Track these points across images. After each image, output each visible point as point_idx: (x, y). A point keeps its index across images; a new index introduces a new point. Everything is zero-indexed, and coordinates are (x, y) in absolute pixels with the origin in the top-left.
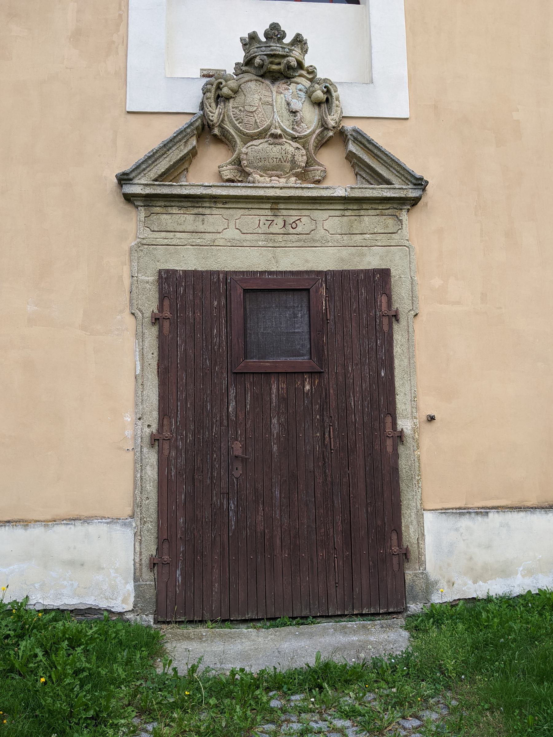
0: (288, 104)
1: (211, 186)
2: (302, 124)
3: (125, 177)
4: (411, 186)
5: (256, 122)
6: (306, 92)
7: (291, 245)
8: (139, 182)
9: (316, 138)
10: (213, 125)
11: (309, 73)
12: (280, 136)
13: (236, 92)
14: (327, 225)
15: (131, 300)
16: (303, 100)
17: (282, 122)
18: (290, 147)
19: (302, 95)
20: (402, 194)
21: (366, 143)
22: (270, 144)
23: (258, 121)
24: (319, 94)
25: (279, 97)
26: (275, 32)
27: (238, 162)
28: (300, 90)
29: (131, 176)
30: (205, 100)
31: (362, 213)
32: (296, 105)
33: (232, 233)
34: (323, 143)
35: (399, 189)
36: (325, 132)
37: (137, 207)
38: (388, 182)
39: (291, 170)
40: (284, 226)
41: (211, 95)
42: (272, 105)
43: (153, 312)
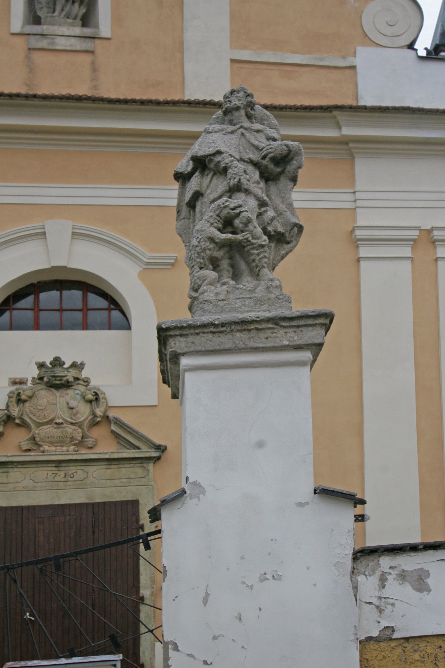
0: (68, 404)
1: (13, 456)
2: (78, 415)
4: (153, 450)
5: (45, 415)
6: (81, 395)
7: (69, 488)
9: (89, 421)
10: (15, 418)
11: (84, 381)
12: (62, 423)
13: (31, 397)
14: (95, 475)
16: (79, 400)
17: (62, 414)
18: (70, 429)
19: (78, 397)
20: (148, 455)
21: (122, 425)
22: (55, 428)
23: (46, 415)
24: (90, 397)
25: (62, 399)
26: (57, 362)
27: (34, 438)
28: (77, 394)
30: (9, 403)
31: (121, 466)
32: (73, 403)
33: (27, 483)
34: (94, 424)
35: (147, 452)
36: (95, 418)
38: (139, 448)
39: (71, 442)
40: (65, 477)
41: (14, 400)
42: (58, 404)
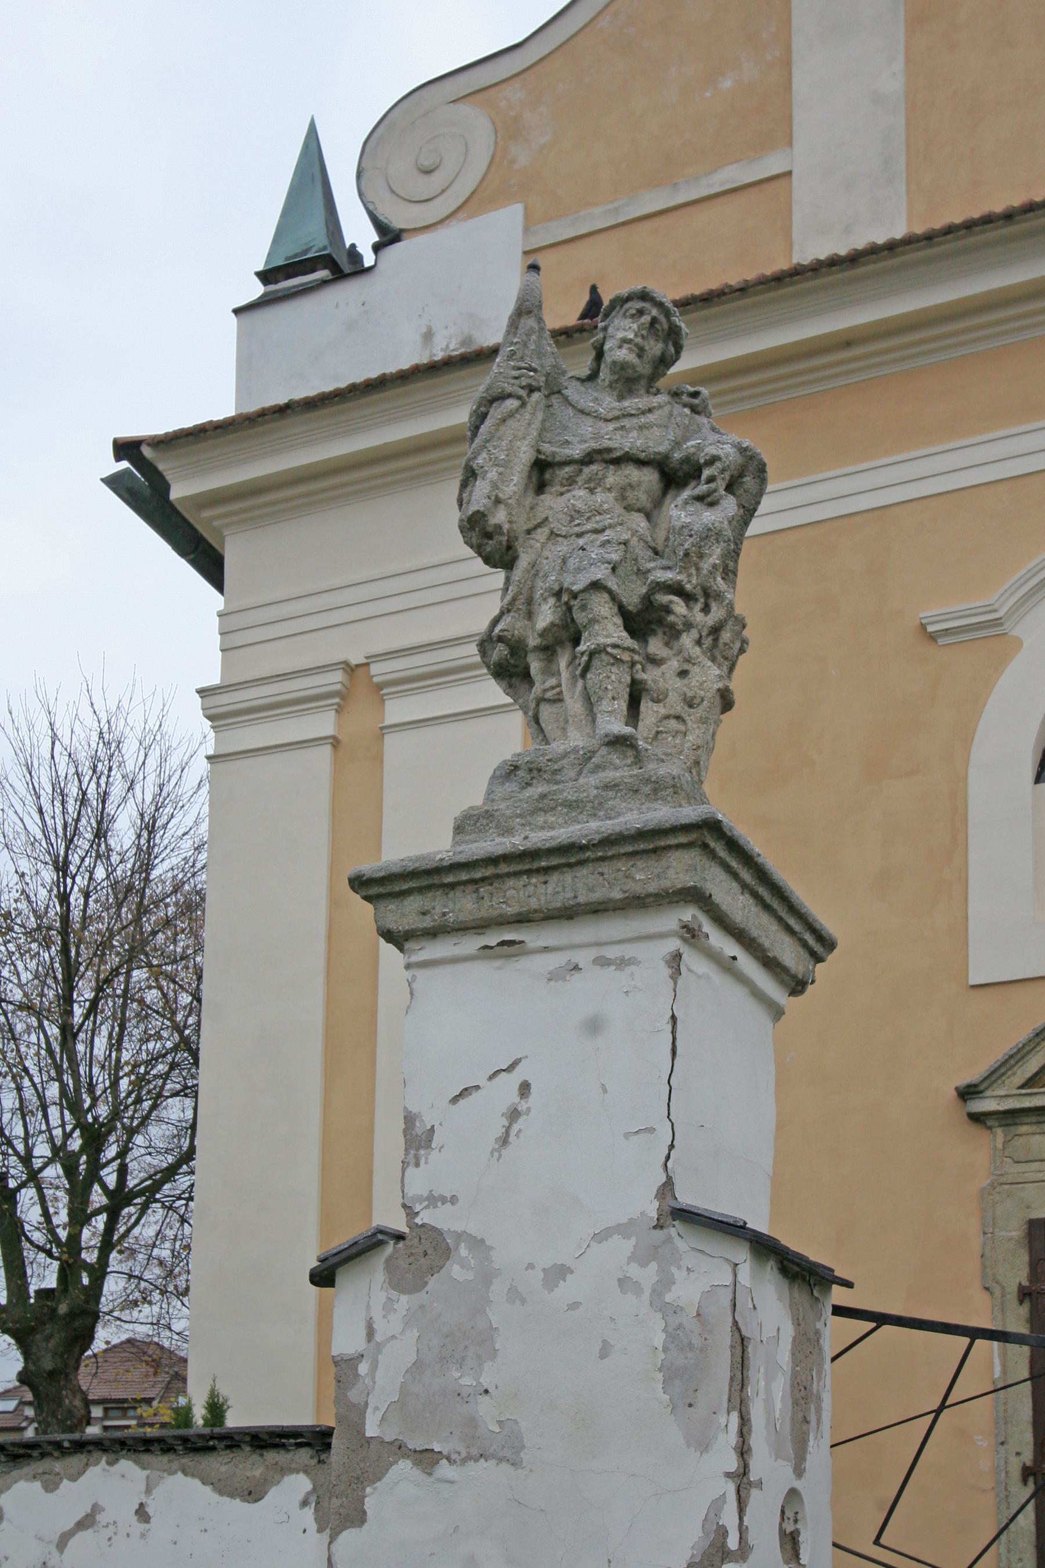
3: (972, 1090)
8: (995, 1093)
15: (984, 1267)
29: (982, 1088)
37: (990, 1128)
43: (1020, 1284)
